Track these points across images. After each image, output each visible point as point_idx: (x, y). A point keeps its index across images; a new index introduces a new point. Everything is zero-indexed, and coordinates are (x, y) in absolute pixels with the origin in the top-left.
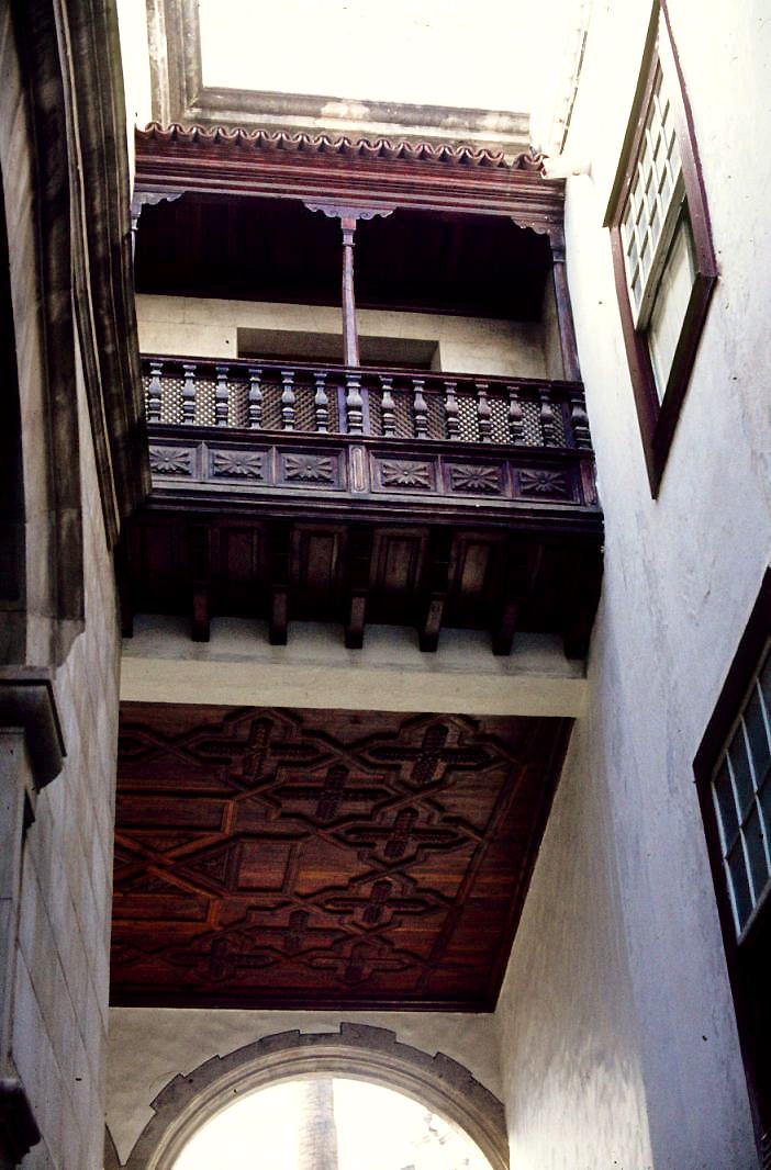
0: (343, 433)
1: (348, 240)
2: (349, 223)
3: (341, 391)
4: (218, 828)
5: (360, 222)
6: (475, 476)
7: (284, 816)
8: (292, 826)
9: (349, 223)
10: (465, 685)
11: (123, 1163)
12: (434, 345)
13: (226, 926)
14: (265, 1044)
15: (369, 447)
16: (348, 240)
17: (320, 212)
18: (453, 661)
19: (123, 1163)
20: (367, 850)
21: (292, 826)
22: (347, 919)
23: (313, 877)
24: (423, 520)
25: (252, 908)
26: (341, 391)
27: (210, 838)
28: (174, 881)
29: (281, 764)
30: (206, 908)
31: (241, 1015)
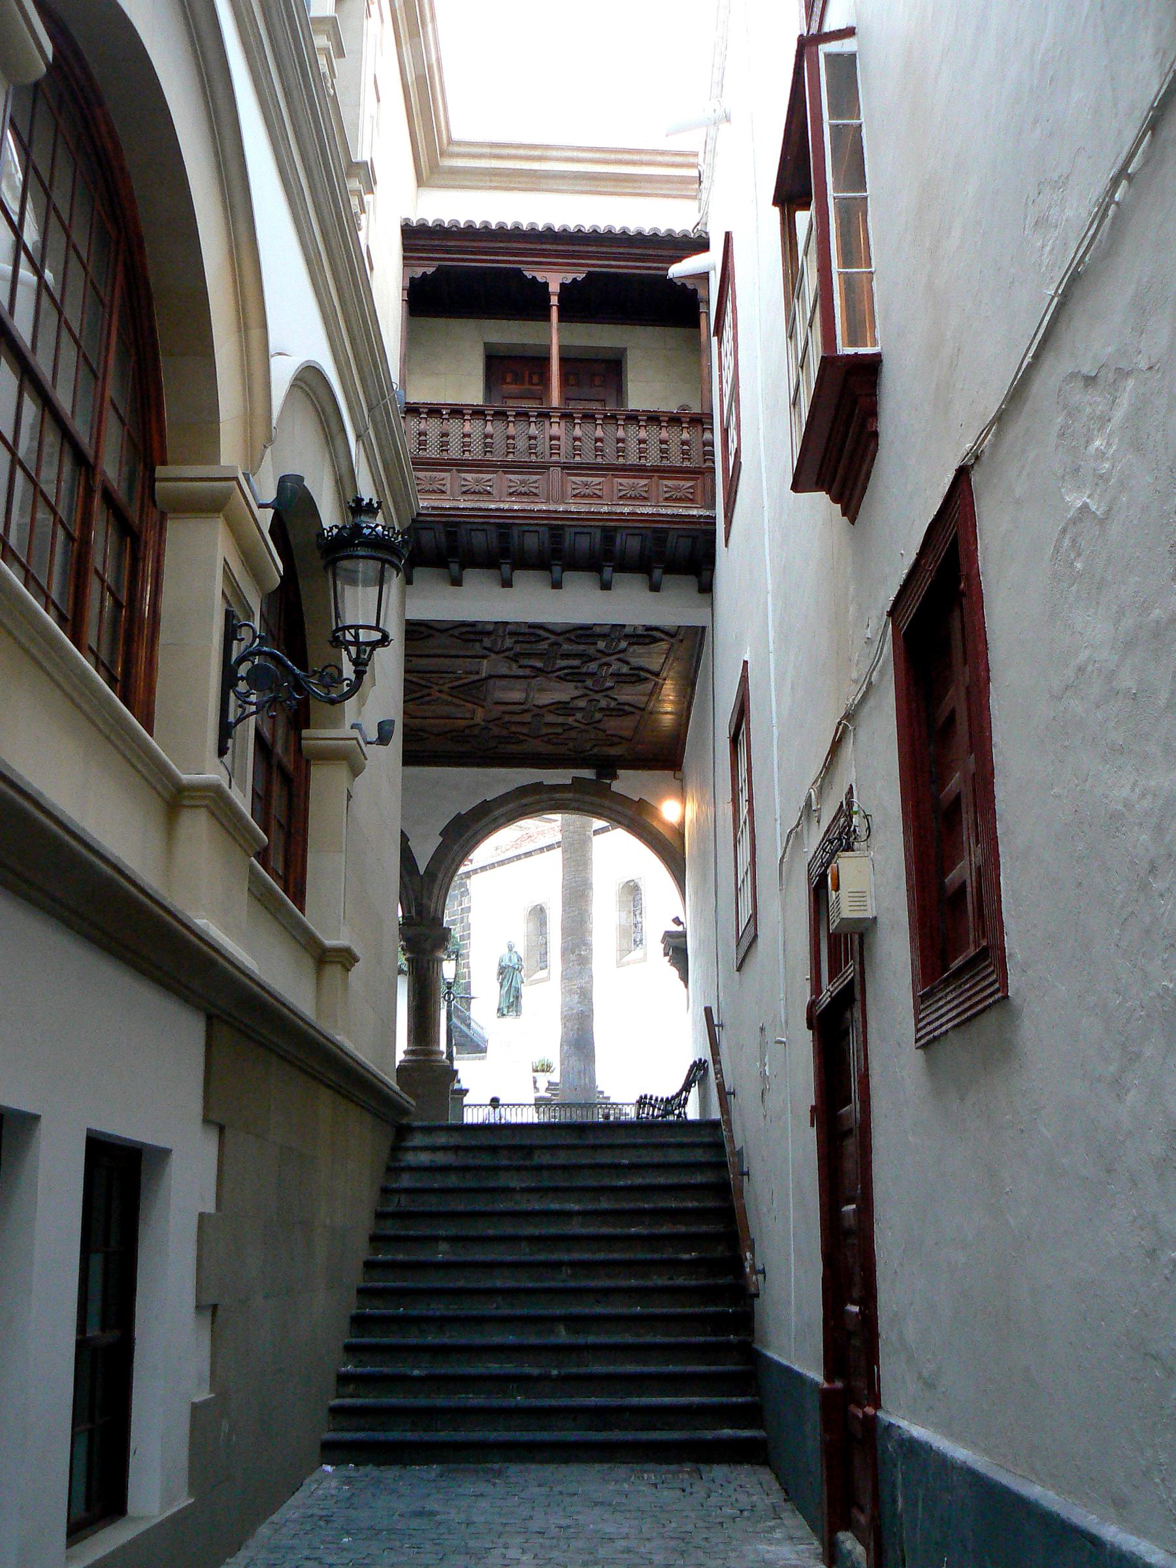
0: (547, 459)
1: (554, 300)
2: (554, 288)
3: (547, 423)
4: (478, 673)
5: (562, 285)
6: (633, 487)
7: (520, 667)
8: (528, 672)
9: (554, 288)
10: (628, 605)
11: (422, 872)
12: (623, 351)
13: (489, 722)
14: (523, 791)
15: (563, 468)
16: (554, 300)
17: (534, 278)
18: (357, 1093)
19: (422, 872)
20: (579, 684)
21: (528, 672)
22: (571, 719)
23: (545, 699)
24: (597, 523)
25: (504, 713)
26: (547, 423)
27: (476, 677)
28: (450, 699)
29: (516, 642)
30: (474, 712)
31: (503, 771)
